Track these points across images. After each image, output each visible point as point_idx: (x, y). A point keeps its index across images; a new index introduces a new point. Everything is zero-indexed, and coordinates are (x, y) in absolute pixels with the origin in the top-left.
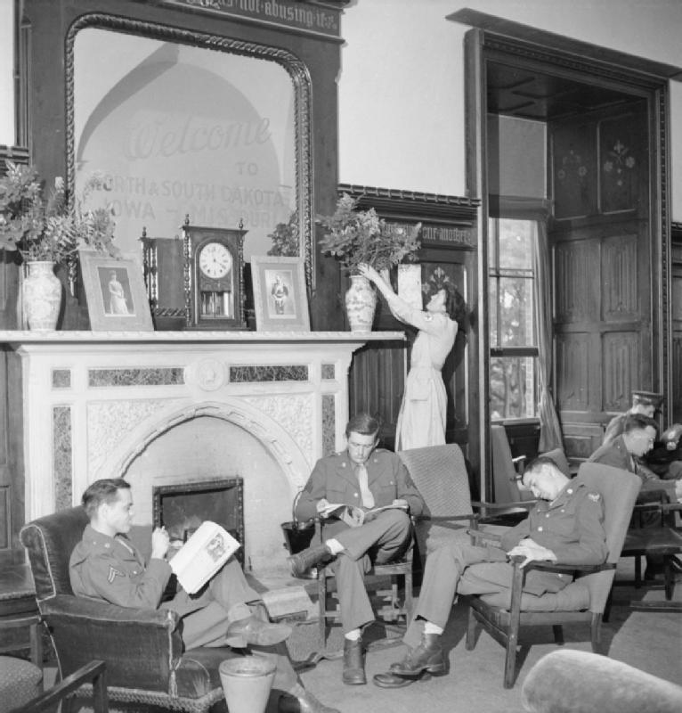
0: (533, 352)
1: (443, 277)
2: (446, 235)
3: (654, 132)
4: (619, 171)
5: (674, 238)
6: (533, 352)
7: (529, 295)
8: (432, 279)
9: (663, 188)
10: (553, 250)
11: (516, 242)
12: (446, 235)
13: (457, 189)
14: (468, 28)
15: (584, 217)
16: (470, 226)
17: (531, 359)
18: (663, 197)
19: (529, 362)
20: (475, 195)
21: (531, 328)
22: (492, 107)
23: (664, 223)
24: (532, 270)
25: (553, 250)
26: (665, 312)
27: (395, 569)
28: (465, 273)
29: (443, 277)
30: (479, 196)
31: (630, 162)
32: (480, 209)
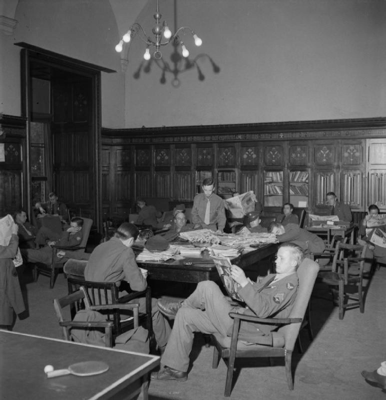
0: (45, 179)
1: (13, 148)
2: (14, 131)
3: (95, 107)
4: (81, 105)
5: (102, 134)
6: (45, 179)
7: (42, 154)
8: (9, 149)
9: (98, 114)
10: (53, 136)
11: (35, 131)
12: (14, 131)
13: (17, 113)
14: (21, 48)
15: (73, 136)
16: (23, 128)
17: (44, 182)
18: (98, 117)
19: (43, 184)
20: (25, 116)
21: (44, 168)
22: (31, 75)
23: (98, 128)
24: (44, 144)
25: (53, 136)
26: (99, 163)
27: (318, 218)
28: (21, 147)
29: (13, 148)
30: (27, 116)
31: (85, 103)
32: (27, 122)
